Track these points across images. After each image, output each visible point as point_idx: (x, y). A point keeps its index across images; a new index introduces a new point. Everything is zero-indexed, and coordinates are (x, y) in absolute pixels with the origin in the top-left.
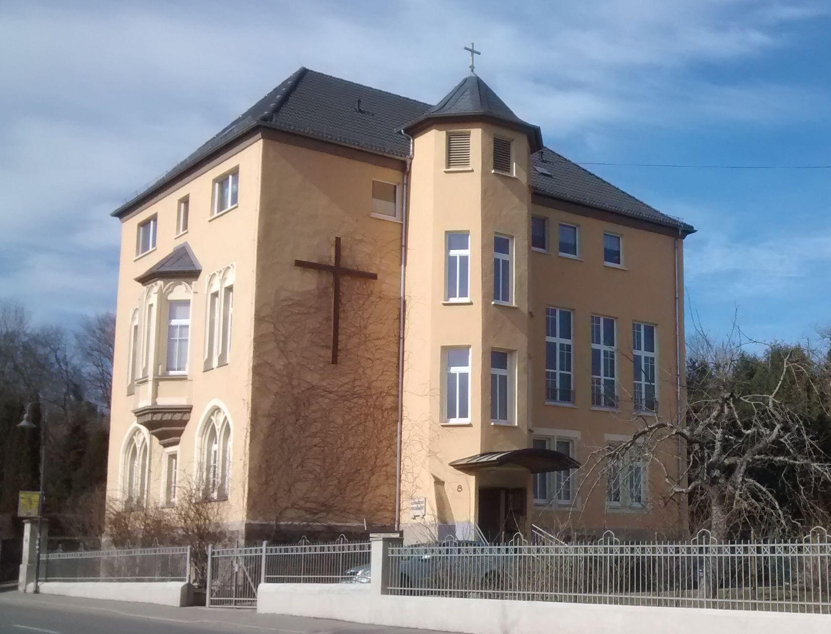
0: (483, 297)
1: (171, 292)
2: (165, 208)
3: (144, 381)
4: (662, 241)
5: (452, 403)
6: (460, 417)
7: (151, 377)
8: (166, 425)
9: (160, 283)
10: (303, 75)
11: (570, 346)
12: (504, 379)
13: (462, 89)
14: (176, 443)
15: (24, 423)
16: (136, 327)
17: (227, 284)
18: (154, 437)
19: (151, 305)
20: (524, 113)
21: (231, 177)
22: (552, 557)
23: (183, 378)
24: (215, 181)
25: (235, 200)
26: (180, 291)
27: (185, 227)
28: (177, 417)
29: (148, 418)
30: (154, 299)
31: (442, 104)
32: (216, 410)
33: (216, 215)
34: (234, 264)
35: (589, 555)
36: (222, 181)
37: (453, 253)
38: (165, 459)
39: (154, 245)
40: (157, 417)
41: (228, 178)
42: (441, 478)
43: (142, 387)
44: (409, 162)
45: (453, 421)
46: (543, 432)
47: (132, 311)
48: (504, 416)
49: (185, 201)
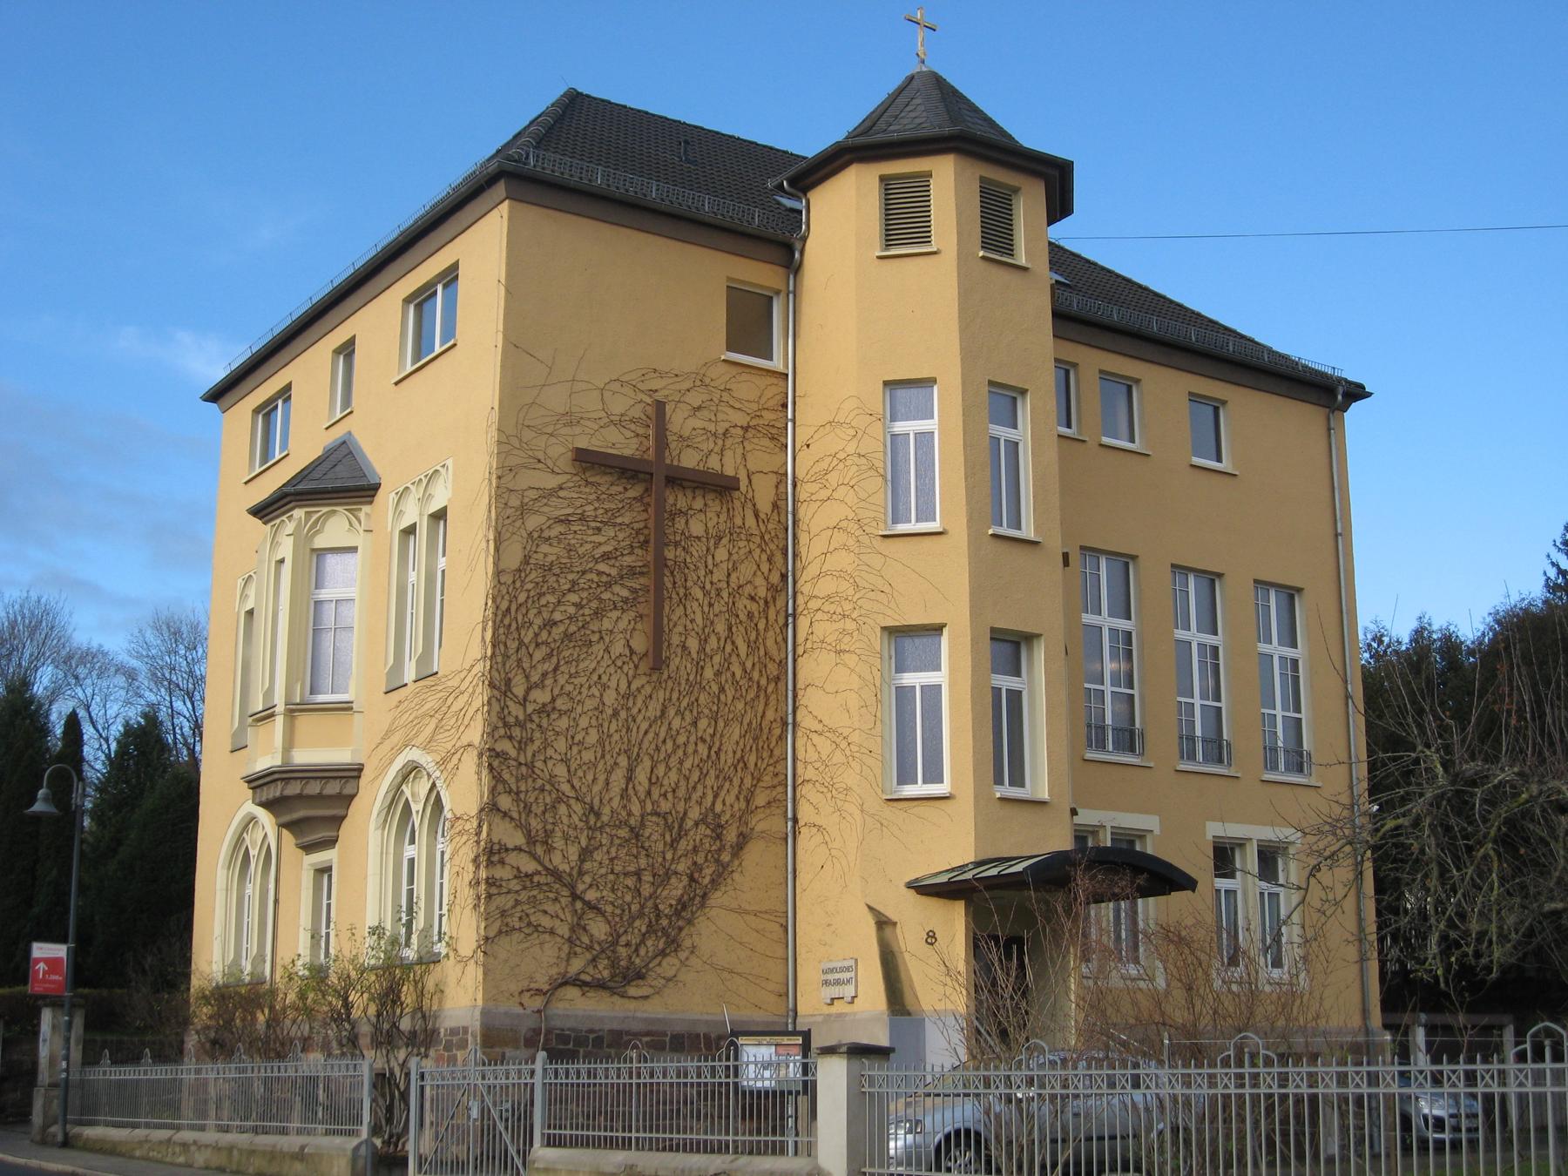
0: (970, 520)
1: (318, 532)
2: (310, 370)
3: (267, 715)
4: (1300, 416)
5: (912, 753)
6: (925, 782)
7: (280, 708)
8: (309, 805)
9: (299, 513)
10: (573, 102)
11: (1129, 634)
12: (1015, 697)
13: (901, 100)
14: (331, 843)
15: (38, 807)
16: (250, 613)
17: (434, 507)
18: (285, 832)
19: (282, 561)
20: (1030, 136)
21: (440, 288)
22: (706, 1084)
23: (346, 707)
24: (407, 301)
25: (449, 330)
26: (337, 527)
27: (347, 401)
28: (333, 788)
29: (274, 792)
30: (286, 549)
31: (868, 123)
32: (411, 771)
33: (409, 369)
34: (450, 462)
35: (1220, 1091)
36: (421, 299)
37: (900, 427)
38: (307, 878)
39: (284, 445)
40: (293, 789)
41: (435, 293)
42: (891, 914)
43: (263, 729)
44: (798, 246)
45: (909, 791)
46: (1087, 817)
47: (240, 582)
48: (1018, 779)
49: (347, 350)
